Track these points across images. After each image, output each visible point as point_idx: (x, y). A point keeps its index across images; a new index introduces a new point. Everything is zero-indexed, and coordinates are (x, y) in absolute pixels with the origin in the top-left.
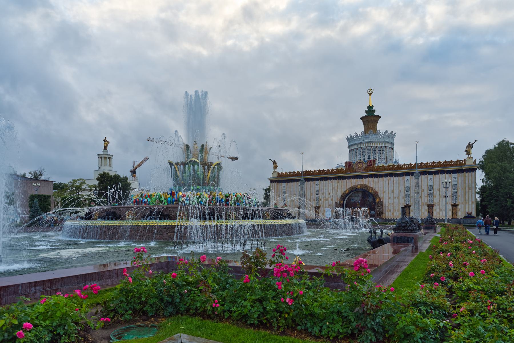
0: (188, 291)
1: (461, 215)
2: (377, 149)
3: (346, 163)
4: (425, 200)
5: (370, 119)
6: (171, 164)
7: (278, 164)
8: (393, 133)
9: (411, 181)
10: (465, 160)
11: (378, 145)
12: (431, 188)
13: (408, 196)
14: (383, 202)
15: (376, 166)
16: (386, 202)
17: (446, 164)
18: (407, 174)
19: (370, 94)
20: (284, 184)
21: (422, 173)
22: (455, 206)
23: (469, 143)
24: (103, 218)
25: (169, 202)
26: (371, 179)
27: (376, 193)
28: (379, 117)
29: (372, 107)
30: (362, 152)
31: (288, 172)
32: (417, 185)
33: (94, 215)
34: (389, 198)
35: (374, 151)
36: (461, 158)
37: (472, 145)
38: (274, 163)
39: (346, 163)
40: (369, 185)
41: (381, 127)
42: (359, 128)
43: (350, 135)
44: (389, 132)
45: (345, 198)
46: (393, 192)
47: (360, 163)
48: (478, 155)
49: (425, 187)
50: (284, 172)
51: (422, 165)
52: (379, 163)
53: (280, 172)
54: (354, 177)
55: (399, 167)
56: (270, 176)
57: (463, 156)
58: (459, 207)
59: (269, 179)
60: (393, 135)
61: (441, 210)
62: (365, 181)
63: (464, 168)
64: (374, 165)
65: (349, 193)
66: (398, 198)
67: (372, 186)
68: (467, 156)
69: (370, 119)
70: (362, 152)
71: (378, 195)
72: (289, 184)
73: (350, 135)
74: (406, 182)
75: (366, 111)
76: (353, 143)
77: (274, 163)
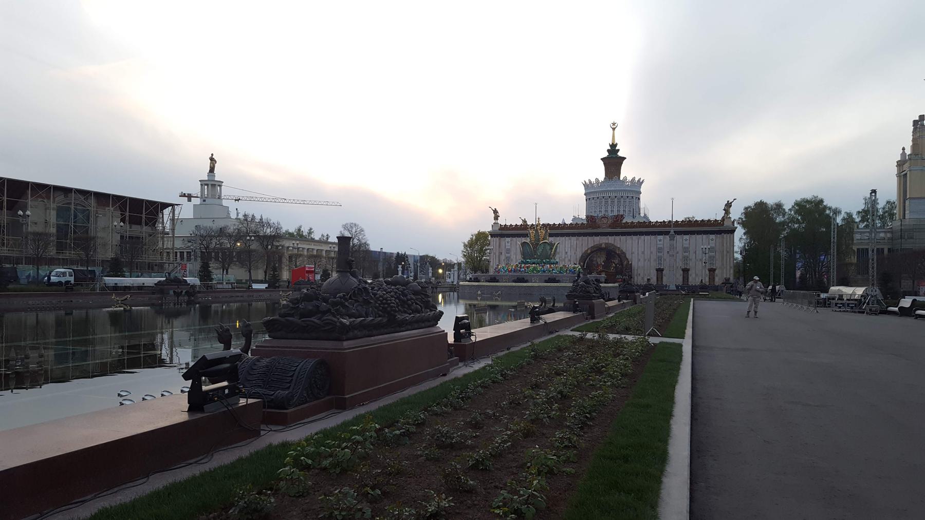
1: (718, 281)
5: (613, 161)
11: (625, 195)
13: (660, 258)
16: (635, 265)
18: (660, 233)
20: (508, 239)
21: (677, 233)
22: (712, 271)
24: (546, 282)
26: (617, 238)
32: (672, 247)
33: (482, 279)
34: (639, 260)
35: (619, 202)
38: (495, 212)
42: (599, 173)
46: (643, 253)
48: (736, 213)
50: (508, 224)
52: (628, 219)
54: (597, 234)
55: (649, 224)
58: (717, 272)
60: (640, 183)
61: (696, 275)
62: (611, 240)
63: (722, 228)
65: (592, 252)
66: (649, 260)
69: (613, 161)
72: (514, 239)
75: (608, 151)
76: (591, 191)
77: (495, 212)
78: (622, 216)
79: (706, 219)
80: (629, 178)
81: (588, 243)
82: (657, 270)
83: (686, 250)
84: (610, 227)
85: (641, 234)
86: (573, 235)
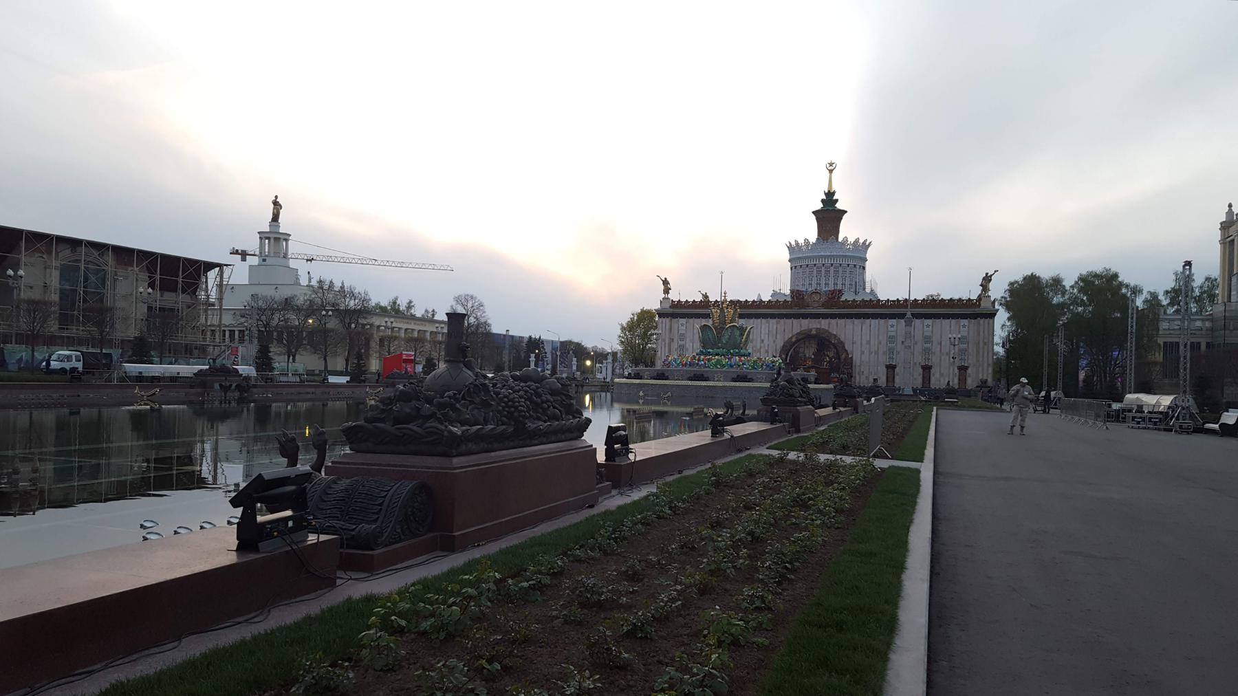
2: (832, 269)
7: (672, 285)
13: (891, 351)
18: (892, 316)
19: (831, 171)
21: (916, 316)
29: (834, 193)
35: (836, 272)
38: (665, 282)
41: (848, 231)
42: (809, 231)
44: (861, 241)
46: (869, 343)
50: (683, 300)
55: (876, 303)
62: (824, 324)
76: (799, 257)
77: (665, 282)
78: (840, 291)
80: (851, 240)
81: (793, 327)
83: (927, 339)
84: (824, 305)
86: (773, 316)
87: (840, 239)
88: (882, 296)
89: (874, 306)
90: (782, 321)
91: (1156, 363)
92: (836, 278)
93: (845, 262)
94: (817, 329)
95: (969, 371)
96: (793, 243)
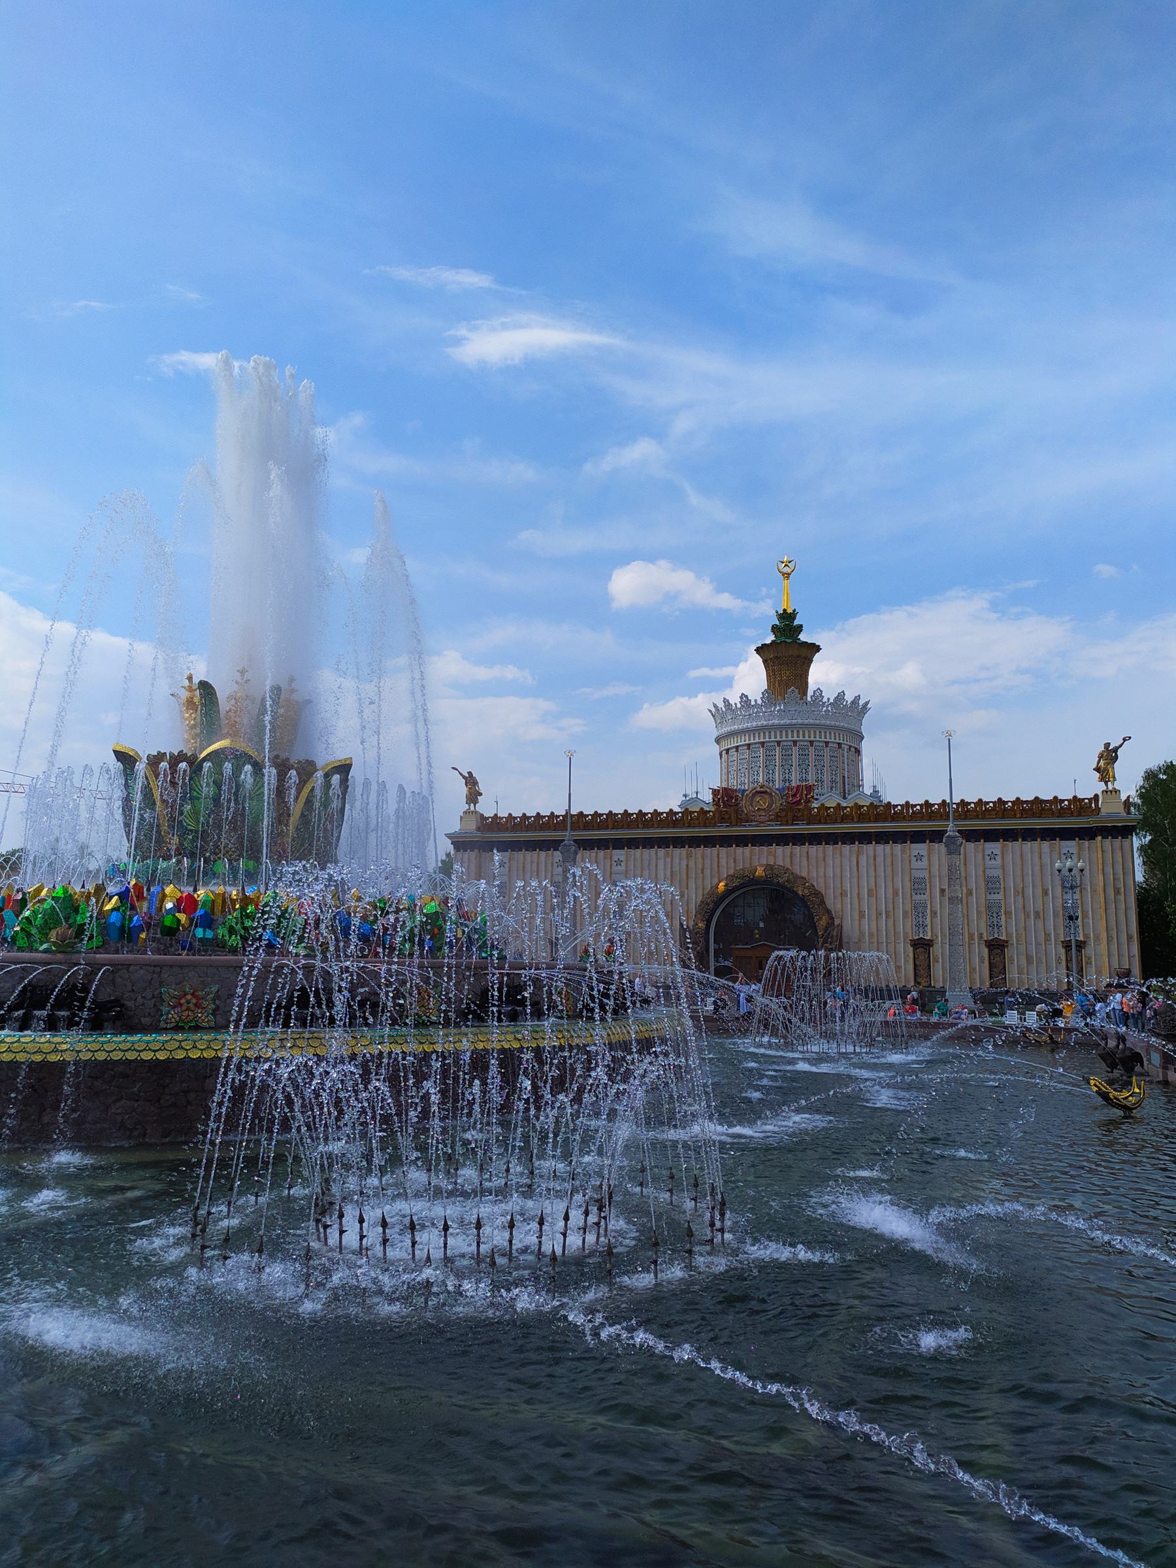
0: (130, 1367)
3: (715, 792)
4: (979, 926)
5: (788, 653)
6: (125, 759)
7: (482, 787)
8: (861, 702)
9: (929, 859)
10: (1096, 796)
12: (992, 884)
13: (919, 909)
14: (841, 926)
15: (815, 805)
17: (1038, 807)
18: (918, 837)
21: (971, 836)
23: (1107, 745)
25: (114, 934)
27: (818, 894)
28: (815, 648)
30: (812, 757)
31: (517, 813)
35: (804, 756)
36: (1085, 793)
37: (1116, 750)
38: (470, 780)
39: (715, 792)
40: (797, 870)
41: (822, 675)
42: (751, 677)
43: (726, 701)
44: (849, 698)
45: (713, 912)
47: (762, 792)
48: (1129, 782)
49: (975, 881)
50: (503, 814)
51: (964, 810)
53: (489, 813)
55: (882, 811)
56: (455, 827)
57: (1089, 787)
59: (449, 836)
60: (858, 709)
62: (780, 855)
64: (808, 801)
67: (804, 874)
68: (1102, 786)
69: (788, 653)
70: (812, 757)
71: (823, 902)
73: (715, 706)
74: (915, 864)
75: (774, 629)
76: (737, 731)
77: (470, 780)
78: (810, 789)
79: (1047, 796)
80: (829, 695)
81: (718, 868)
82: (1067, 946)
83: (992, 884)
84: (778, 818)
85: (865, 838)
86: (678, 842)
87: (810, 693)
88: (895, 796)
89: (878, 818)
90: (699, 851)
91: (195, 890)
92: (803, 766)
93: (831, 739)
94: (768, 867)
95: (1089, 951)
96: (849, 698)
